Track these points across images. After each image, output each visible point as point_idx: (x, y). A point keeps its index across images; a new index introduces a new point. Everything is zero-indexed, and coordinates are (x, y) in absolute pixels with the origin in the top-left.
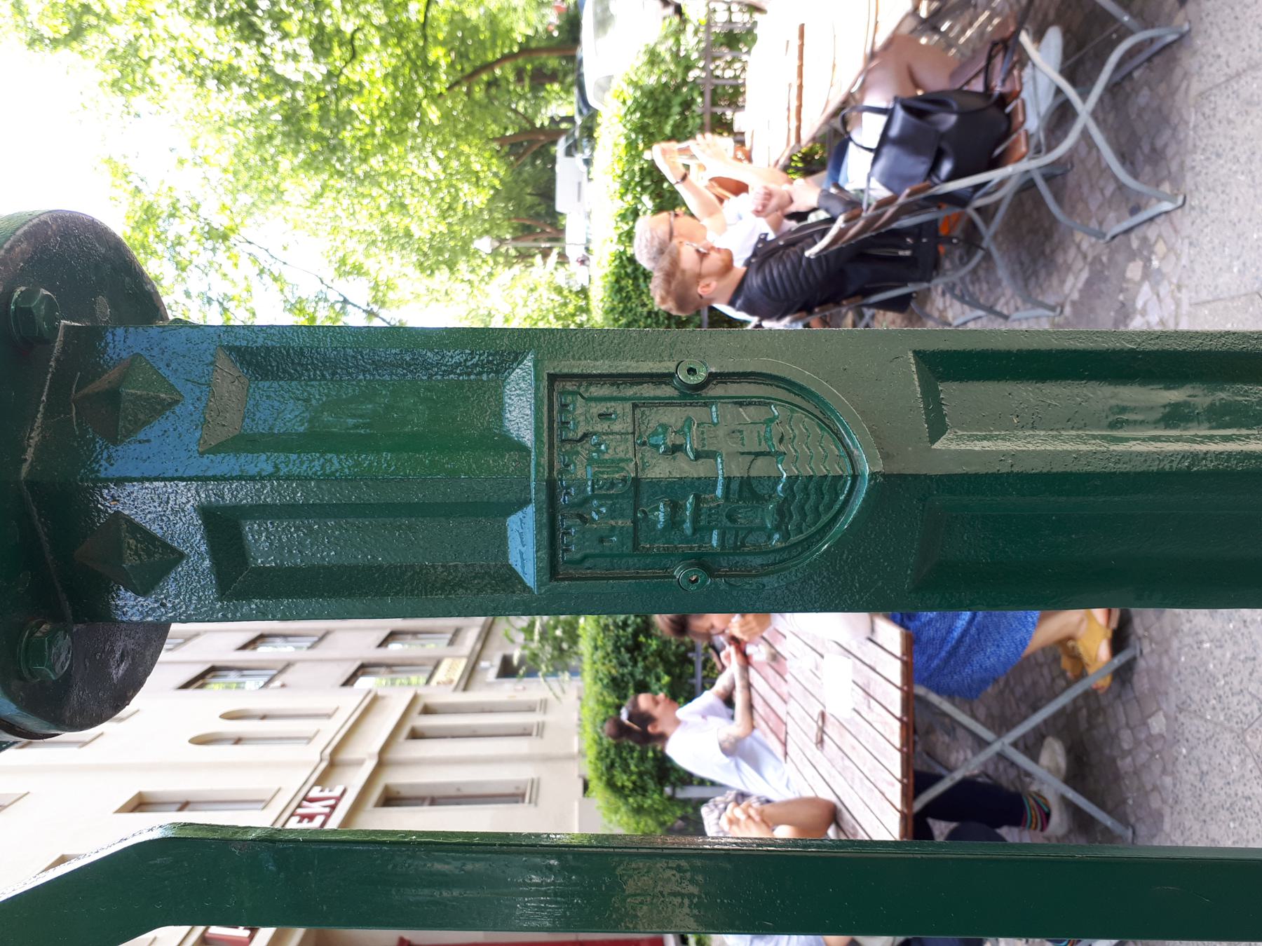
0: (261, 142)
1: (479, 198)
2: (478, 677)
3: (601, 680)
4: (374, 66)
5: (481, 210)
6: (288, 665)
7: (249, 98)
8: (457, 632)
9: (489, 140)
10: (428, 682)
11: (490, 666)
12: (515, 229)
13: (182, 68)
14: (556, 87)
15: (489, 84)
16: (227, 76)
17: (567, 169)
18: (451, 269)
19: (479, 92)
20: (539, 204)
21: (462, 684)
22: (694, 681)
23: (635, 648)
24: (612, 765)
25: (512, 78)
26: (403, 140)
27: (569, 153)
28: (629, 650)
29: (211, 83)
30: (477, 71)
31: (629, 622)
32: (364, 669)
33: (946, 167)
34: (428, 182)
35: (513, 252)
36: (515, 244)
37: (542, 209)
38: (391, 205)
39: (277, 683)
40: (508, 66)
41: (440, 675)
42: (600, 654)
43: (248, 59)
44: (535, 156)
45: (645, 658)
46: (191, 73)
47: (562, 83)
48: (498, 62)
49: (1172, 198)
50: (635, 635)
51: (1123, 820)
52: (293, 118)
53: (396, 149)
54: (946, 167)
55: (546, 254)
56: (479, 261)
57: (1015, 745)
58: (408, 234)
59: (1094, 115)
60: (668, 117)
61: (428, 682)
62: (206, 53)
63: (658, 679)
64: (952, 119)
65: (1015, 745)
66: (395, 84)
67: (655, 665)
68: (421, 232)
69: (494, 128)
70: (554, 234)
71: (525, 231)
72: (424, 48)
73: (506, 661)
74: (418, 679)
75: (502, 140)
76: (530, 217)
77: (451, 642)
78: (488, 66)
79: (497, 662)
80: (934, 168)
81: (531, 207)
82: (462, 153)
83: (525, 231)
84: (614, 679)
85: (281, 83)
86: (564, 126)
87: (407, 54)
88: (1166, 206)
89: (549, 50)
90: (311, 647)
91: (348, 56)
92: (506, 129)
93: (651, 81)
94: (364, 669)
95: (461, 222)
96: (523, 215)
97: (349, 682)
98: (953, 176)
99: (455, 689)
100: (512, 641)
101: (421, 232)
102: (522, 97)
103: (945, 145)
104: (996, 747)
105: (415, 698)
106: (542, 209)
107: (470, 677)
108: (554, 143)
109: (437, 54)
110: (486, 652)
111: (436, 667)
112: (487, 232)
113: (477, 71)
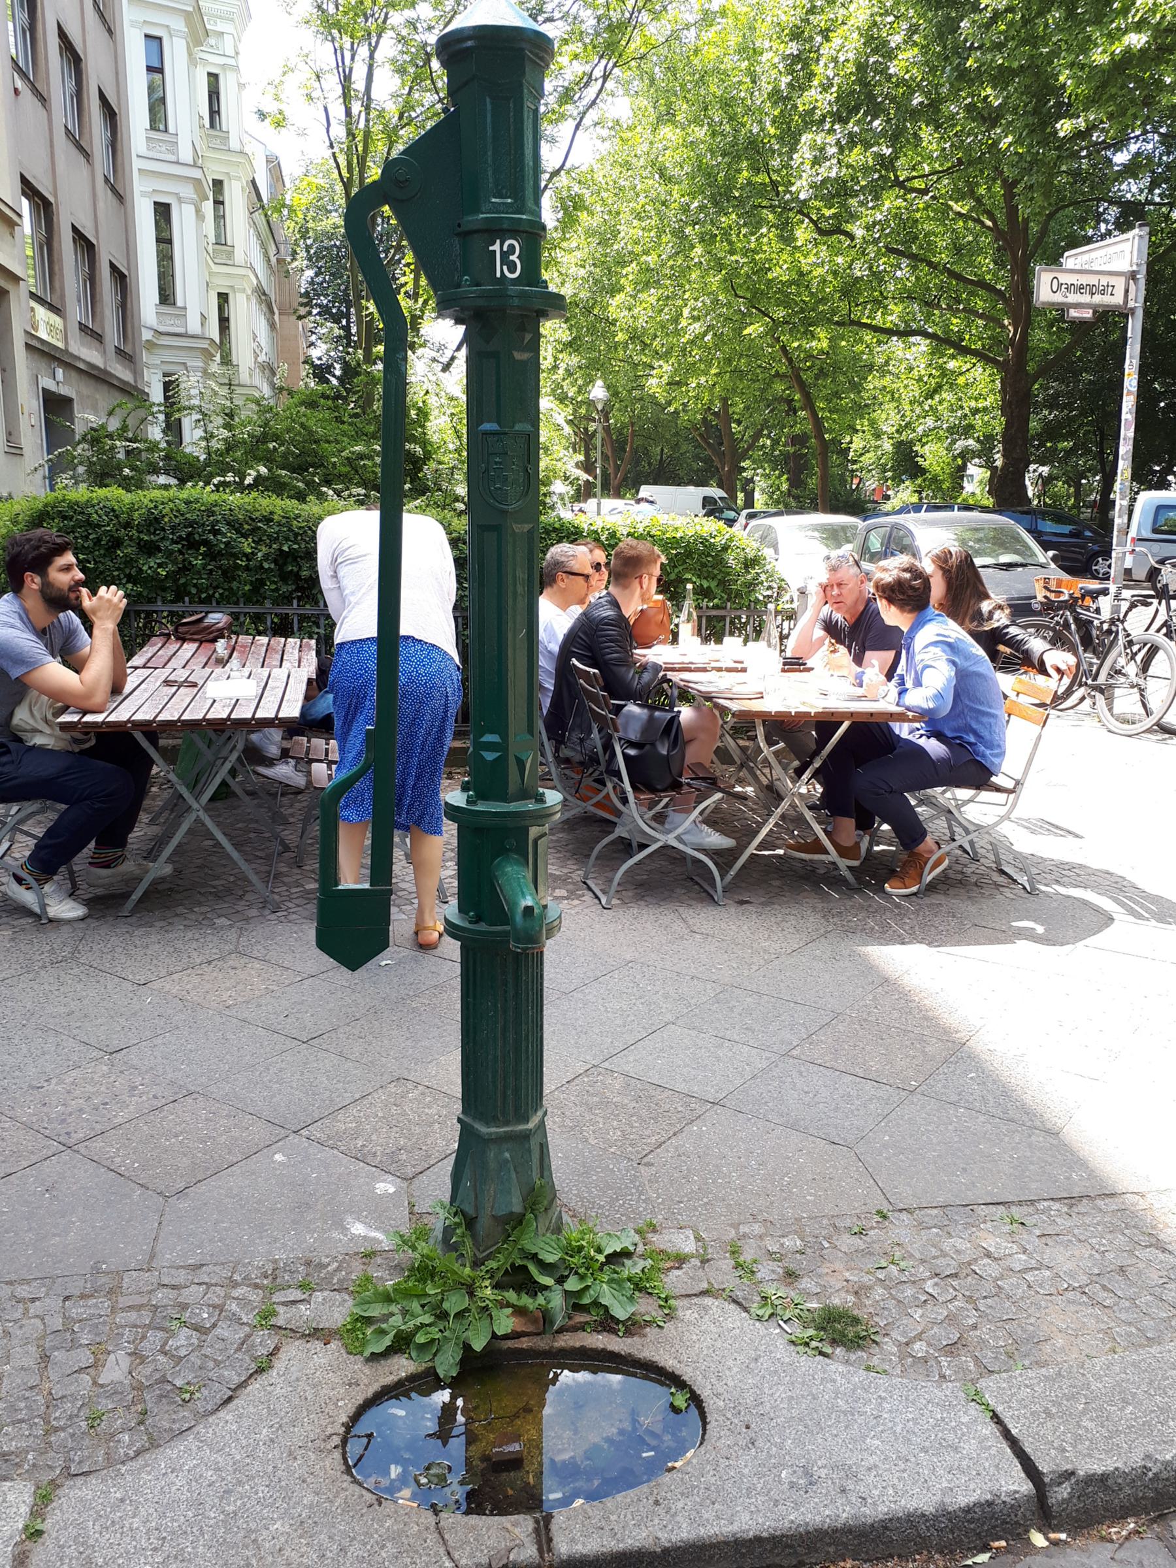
0: (727, 104)
1: (654, 385)
2: (43, 365)
3: (156, 507)
4: (812, 258)
5: (642, 387)
6: (43, 100)
7: (776, 96)
8: (98, 337)
9: (724, 400)
10: (33, 296)
11: (59, 382)
12: (620, 432)
13: (812, 11)
14: (785, 487)
15: (790, 401)
16: (800, 65)
17: (693, 495)
18: (570, 344)
19: (779, 387)
20: (650, 464)
21: (34, 343)
22: (159, 603)
23: (192, 544)
24: (65, 518)
25: (797, 429)
26: (725, 290)
27: (707, 501)
28: (190, 534)
29: (793, 48)
30: (803, 386)
31: (219, 537)
32: (43, 207)
33: (632, 752)
34: (676, 320)
35: (592, 427)
36: (600, 429)
37: (645, 466)
38: (648, 269)
39: (19, 84)
40: (809, 427)
41: (41, 312)
42: (183, 507)
43: (816, 98)
44: (707, 461)
45: (180, 552)
46: (808, 21)
47: (789, 493)
48: (814, 414)
49: (608, 902)
50: (206, 543)
51: (133, 912)
52: (754, 151)
53: (715, 280)
54: (632, 752)
55: (588, 467)
56: (580, 382)
57: (198, 820)
58: (614, 290)
59: (666, 847)
60: (699, 577)
61: (33, 296)
62: (826, 45)
63: (160, 565)
64: (665, 752)
65: (198, 820)
66: (791, 283)
67: (175, 562)
68: (616, 306)
69: (738, 406)
70: (614, 482)
71: (617, 443)
72: (829, 321)
73: (66, 402)
74: (31, 282)
75: (725, 416)
76: (635, 451)
77: (83, 328)
78: (809, 404)
79: (64, 390)
80: (632, 744)
81: (646, 452)
82: (710, 365)
83: (617, 443)
84: (157, 520)
85: (790, 138)
86: (741, 496)
87: (823, 301)
88: (604, 902)
89: (825, 477)
90: (68, 132)
91: (824, 225)
92: (739, 422)
93: (731, 559)
94: (43, 207)
95: (628, 360)
96: (638, 441)
97: (28, 189)
98: (625, 755)
99: (27, 332)
100: (110, 414)
101: (616, 306)
102: (776, 442)
103: (647, 747)
104: (195, 806)
105: (16, 279)
106: (645, 466)
107: (41, 351)
108: (720, 486)
109: (821, 341)
110: (74, 374)
111: (52, 308)
112: (615, 394)
113: (803, 386)
